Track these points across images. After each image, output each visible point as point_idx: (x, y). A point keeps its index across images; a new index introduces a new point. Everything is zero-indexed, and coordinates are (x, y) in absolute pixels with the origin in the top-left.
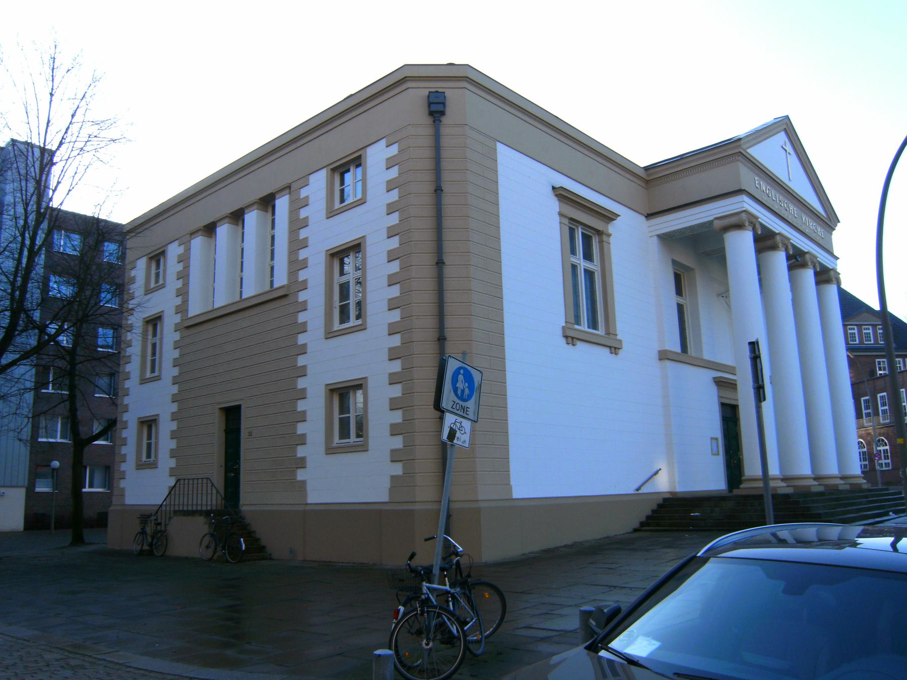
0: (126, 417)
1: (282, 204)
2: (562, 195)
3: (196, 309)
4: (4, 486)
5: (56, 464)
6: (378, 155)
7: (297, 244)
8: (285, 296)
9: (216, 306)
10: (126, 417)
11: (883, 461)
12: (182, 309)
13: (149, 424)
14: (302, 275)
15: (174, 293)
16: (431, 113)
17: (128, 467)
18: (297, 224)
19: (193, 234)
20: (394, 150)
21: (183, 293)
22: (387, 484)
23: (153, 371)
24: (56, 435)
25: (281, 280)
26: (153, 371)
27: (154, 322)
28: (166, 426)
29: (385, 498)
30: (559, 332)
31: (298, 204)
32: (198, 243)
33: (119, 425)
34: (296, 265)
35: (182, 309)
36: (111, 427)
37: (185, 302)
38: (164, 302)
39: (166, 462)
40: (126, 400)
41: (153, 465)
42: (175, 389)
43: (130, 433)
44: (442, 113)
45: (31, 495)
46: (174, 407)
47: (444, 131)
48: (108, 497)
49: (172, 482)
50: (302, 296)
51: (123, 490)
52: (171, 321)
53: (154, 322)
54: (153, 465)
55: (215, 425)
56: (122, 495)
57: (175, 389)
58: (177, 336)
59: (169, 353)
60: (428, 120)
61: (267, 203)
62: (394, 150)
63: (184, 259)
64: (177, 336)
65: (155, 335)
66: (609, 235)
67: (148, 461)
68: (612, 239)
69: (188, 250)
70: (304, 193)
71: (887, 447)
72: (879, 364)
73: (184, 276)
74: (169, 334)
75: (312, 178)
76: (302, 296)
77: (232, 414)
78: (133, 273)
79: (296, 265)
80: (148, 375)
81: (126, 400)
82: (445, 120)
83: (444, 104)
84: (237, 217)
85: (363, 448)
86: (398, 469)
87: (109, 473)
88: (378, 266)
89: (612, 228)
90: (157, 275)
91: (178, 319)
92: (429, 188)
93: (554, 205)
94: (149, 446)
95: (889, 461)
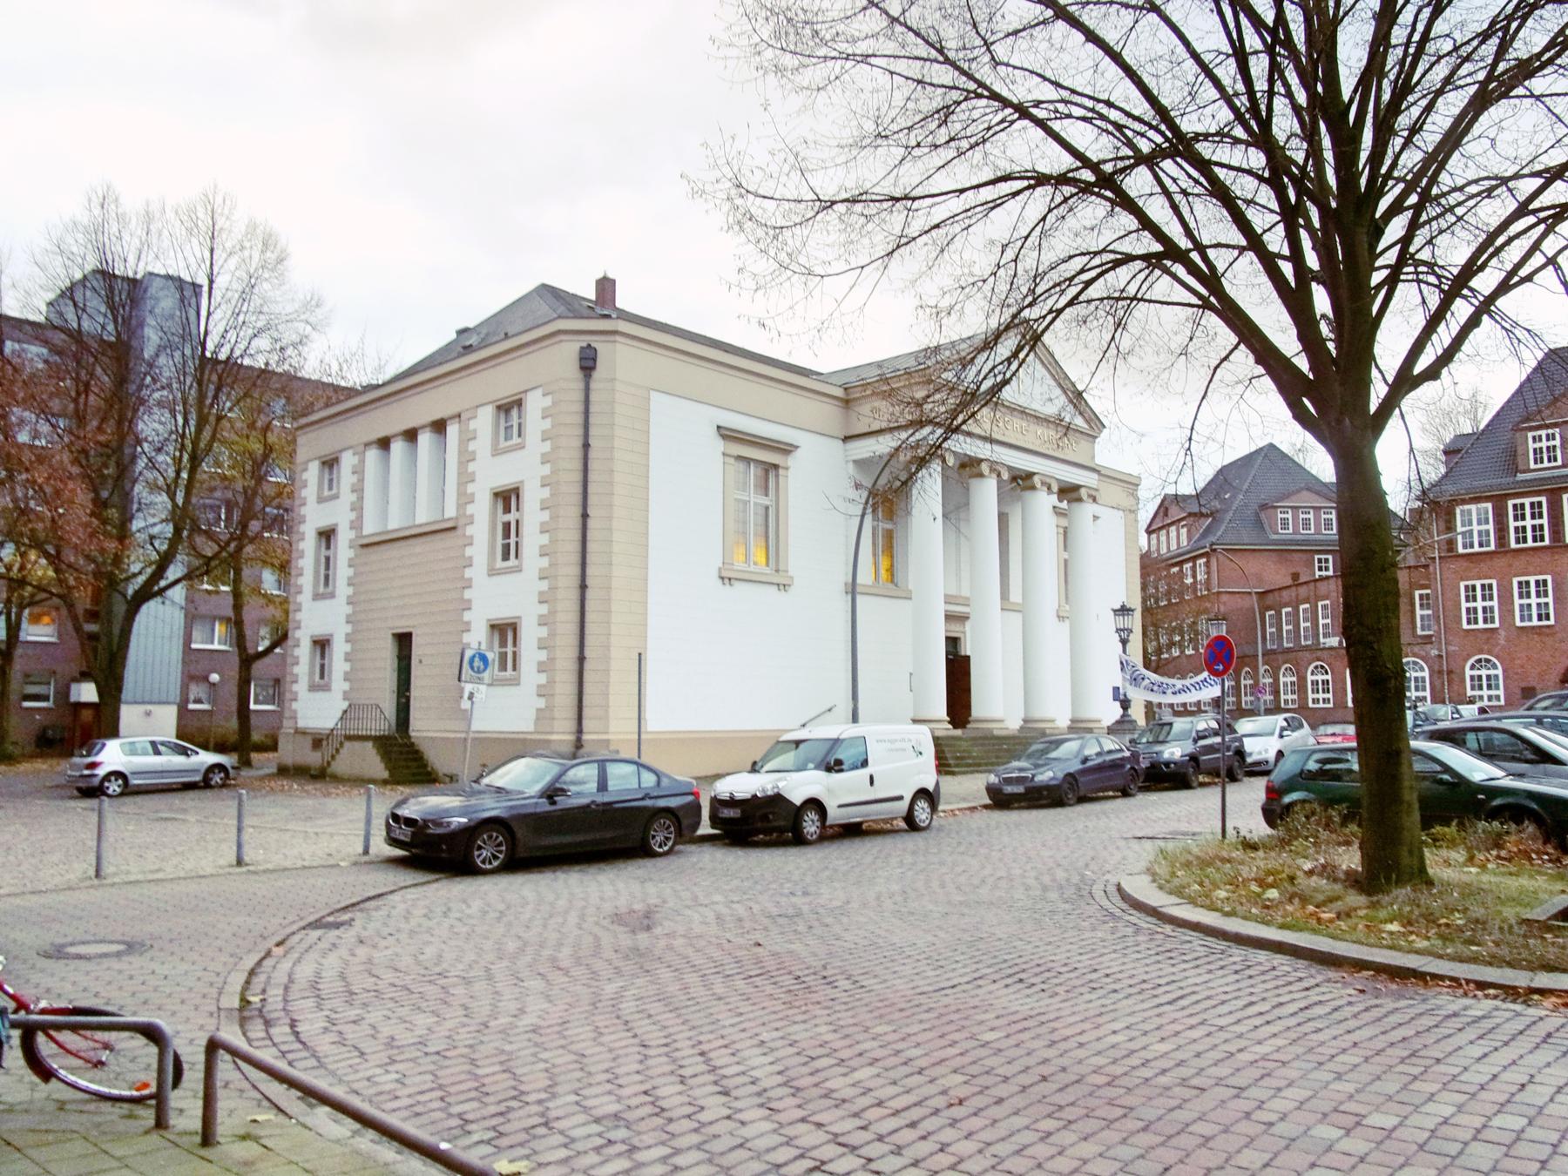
0: (298, 634)
1: (452, 430)
2: (726, 434)
3: (370, 528)
4: (151, 703)
5: (215, 677)
6: (535, 404)
7: (466, 478)
8: (454, 528)
9: (390, 527)
10: (298, 634)
11: (1290, 697)
12: (357, 525)
13: (322, 645)
14: (470, 509)
15: (348, 507)
16: (582, 368)
17: (301, 688)
18: (467, 457)
19: (367, 445)
20: (548, 401)
21: (358, 507)
22: (532, 714)
23: (330, 488)
24: (217, 640)
25: (451, 512)
26: (330, 488)
27: (327, 535)
28: (339, 648)
29: (531, 729)
30: (716, 574)
31: (467, 438)
32: (373, 454)
33: (290, 642)
34: (465, 499)
35: (357, 525)
36: (281, 638)
37: (360, 517)
38: (338, 514)
39: (339, 684)
40: (299, 616)
41: (326, 688)
42: (349, 610)
43: (303, 651)
44: (593, 368)
45: (183, 711)
46: (349, 629)
47: (593, 385)
48: (279, 715)
49: (345, 705)
50: (469, 531)
51: (295, 712)
52: (344, 537)
53: (327, 535)
54: (326, 688)
55: (387, 653)
56: (295, 718)
57: (349, 610)
58: (351, 553)
59: (342, 572)
60: (579, 375)
61: (439, 426)
62: (548, 401)
63: (359, 471)
64: (351, 553)
65: (328, 547)
66: (787, 469)
67: (321, 681)
68: (791, 473)
69: (362, 461)
70: (473, 425)
71: (1329, 677)
72: (1320, 561)
73: (358, 489)
74: (343, 550)
75: (481, 411)
76: (469, 531)
77: (404, 641)
78: (305, 476)
79: (465, 499)
80: (326, 493)
81: (299, 616)
82: (596, 375)
83: (595, 360)
84: (411, 435)
85: (515, 682)
86: (541, 703)
87: (278, 687)
88: (531, 514)
89: (791, 461)
90: (331, 481)
91: (352, 534)
92: (578, 443)
93: (720, 445)
94: (322, 666)
95: (1330, 696)
